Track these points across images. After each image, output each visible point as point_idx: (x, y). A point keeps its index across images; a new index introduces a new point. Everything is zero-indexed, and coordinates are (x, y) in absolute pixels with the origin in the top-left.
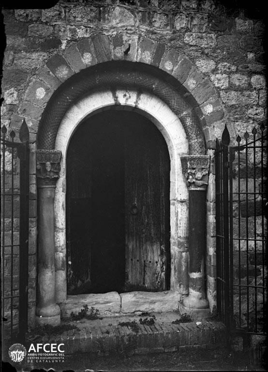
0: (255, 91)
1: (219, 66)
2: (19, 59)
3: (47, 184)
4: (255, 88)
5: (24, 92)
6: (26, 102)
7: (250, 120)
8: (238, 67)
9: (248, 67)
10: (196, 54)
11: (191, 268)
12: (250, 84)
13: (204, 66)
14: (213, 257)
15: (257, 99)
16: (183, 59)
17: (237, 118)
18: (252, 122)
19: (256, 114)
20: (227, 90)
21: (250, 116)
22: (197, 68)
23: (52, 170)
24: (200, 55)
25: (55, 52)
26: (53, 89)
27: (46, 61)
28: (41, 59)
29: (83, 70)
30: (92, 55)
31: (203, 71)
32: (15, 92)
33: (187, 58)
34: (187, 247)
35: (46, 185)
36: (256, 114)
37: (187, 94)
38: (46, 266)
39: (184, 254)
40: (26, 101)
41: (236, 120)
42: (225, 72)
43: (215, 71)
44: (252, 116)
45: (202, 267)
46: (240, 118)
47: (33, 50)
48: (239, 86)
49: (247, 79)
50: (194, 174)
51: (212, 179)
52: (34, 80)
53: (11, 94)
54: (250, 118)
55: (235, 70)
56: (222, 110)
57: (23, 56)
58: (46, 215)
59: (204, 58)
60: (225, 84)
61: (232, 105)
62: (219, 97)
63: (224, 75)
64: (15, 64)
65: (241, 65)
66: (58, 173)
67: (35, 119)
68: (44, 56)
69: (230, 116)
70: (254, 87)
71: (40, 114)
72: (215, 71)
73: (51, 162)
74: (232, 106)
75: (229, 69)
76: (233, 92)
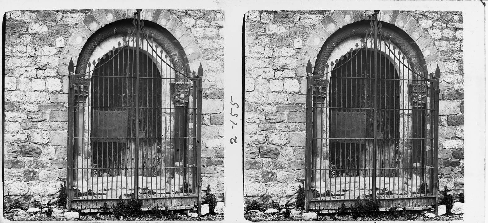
0: (458, 41)
1: (435, 24)
2: (66, 18)
3: (81, 100)
4: (458, 39)
5: (69, 39)
6: (70, 46)
7: (217, 59)
8: (447, 25)
9: (217, 23)
10: (419, 16)
11: (175, 159)
12: (455, 36)
13: (425, 24)
14: (191, 152)
15: (460, 47)
16: (173, 18)
17: (446, 60)
18: (456, 62)
19: (459, 57)
20: (439, 40)
21: (455, 58)
22: (420, 25)
23: (323, 92)
24: (422, 17)
25: (89, 13)
26: (88, 36)
27: (83, 19)
28: (317, 19)
29: (344, 26)
30: (351, 16)
31: (424, 28)
32: (301, 40)
33: (413, 18)
34: (173, 146)
35: (318, 101)
36: (459, 57)
37: (413, 42)
38: (318, 156)
39: (409, 151)
40: (70, 45)
41: (445, 60)
42: (439, 28)
43: (432, 27)
44: (456, 58)
45: (421, 160)
46: (449, 59)
47: (312, 13)
48: (448, 38)
49: (453, 33)
50: (179, 95)
51: (191, 98)
52: (75, 32)
53: (298, 41)
54: (455, 59)
55: (445, 27)
56: (199, 52)
57: (68, 16)
58: (319, 122)
59: (425, 18)
60: (438, 36)
61: (443, 50)
62: (434, 45)
63: (438, 31)
64: (301, 22)
65: (450, 24)
66: (325, 94)
67: (75, 57)
68: (320, 17)
69: (441, 58)
70: (458, 38)
71: (79, 54)
72: (432, 27)
73: (85, 85)
74: (443, 51)
75: (441, 26)
76: (444, 42)
